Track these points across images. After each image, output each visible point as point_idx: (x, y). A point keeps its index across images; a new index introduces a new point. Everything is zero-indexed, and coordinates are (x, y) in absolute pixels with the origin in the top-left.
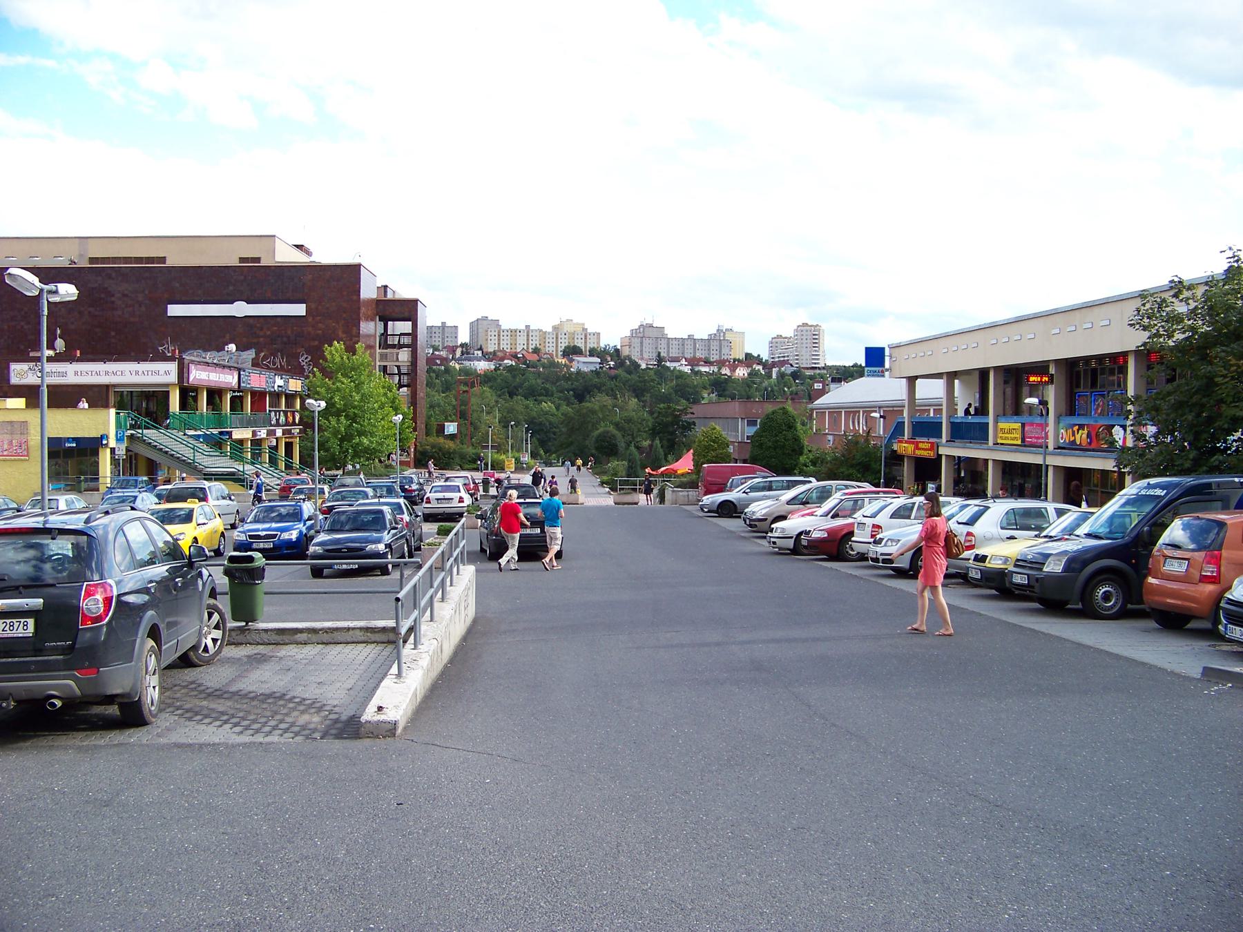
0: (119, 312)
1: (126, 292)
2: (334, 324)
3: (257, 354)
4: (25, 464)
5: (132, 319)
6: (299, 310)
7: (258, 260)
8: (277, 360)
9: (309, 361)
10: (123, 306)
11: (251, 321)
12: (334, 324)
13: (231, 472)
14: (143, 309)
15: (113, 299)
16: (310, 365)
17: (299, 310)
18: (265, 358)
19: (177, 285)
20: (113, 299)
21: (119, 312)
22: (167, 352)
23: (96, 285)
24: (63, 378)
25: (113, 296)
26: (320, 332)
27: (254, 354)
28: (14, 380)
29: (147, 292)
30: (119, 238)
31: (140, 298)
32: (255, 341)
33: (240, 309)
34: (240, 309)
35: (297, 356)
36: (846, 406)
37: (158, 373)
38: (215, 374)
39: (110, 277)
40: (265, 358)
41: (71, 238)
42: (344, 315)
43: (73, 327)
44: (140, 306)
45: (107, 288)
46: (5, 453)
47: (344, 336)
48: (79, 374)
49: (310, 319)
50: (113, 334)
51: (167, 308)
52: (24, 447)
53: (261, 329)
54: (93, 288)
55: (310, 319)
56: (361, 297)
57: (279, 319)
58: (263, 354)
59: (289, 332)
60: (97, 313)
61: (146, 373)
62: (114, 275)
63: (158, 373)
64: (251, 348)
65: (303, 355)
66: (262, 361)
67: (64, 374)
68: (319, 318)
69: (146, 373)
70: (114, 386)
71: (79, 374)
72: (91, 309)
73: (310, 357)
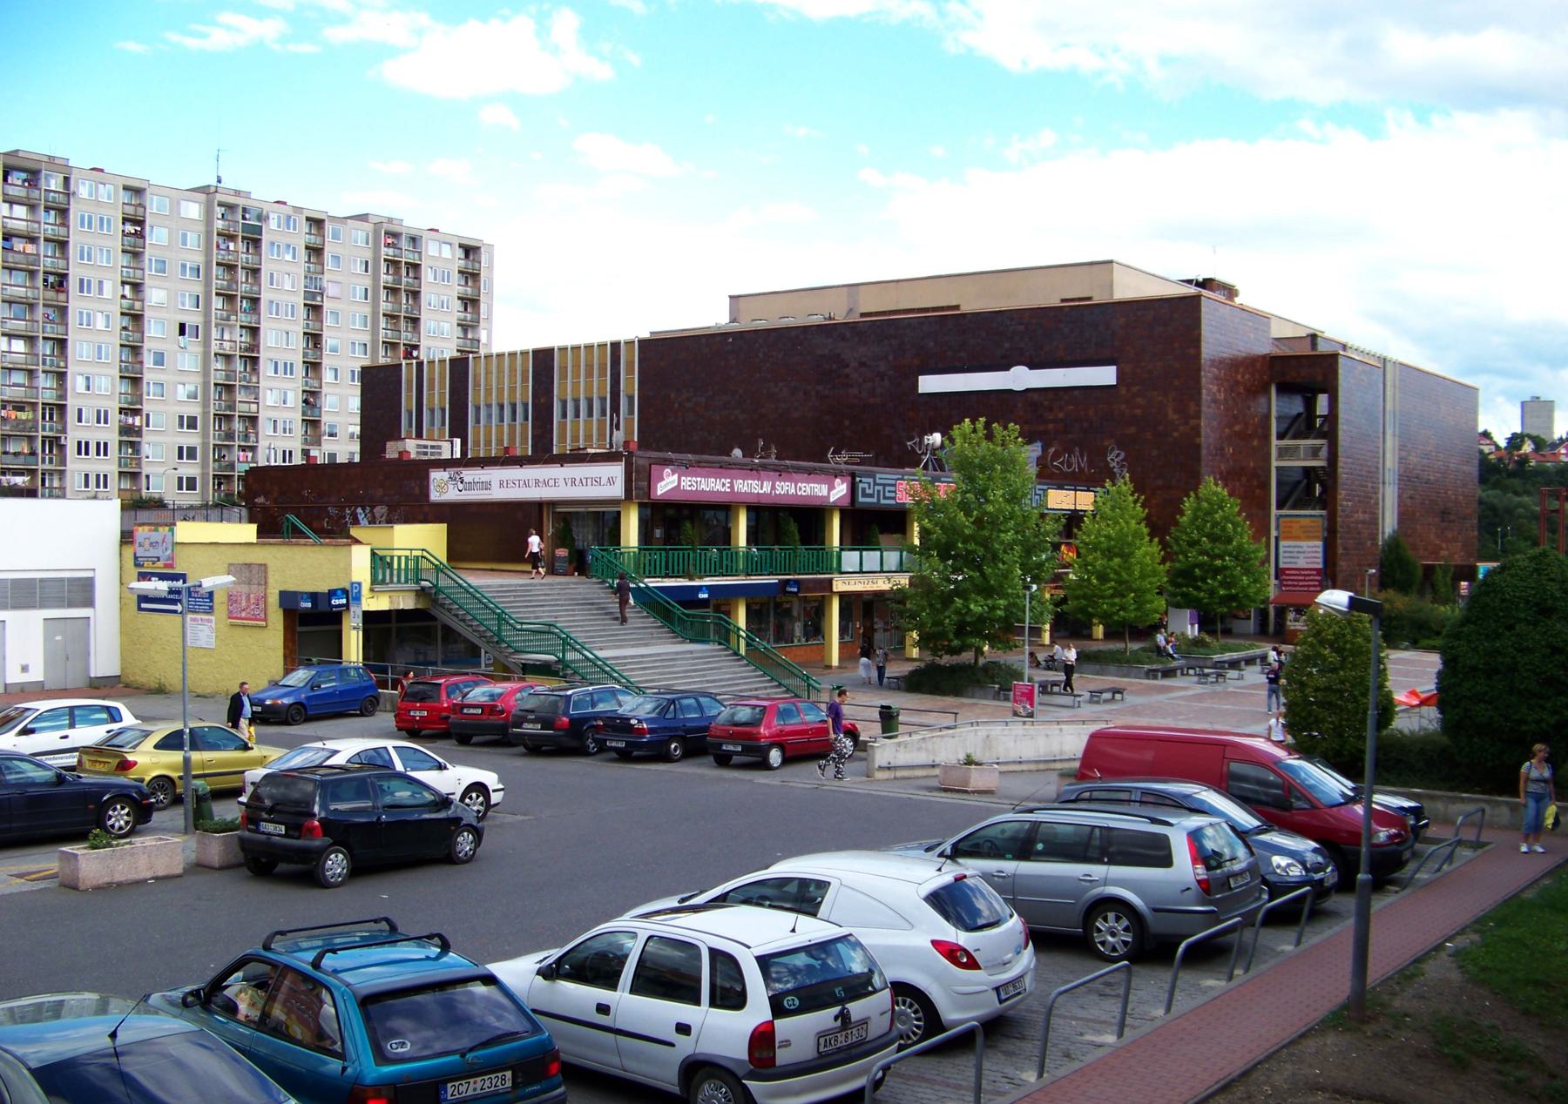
0: (855, 391)
1: (864, 360)
2: (1160, 398)
3: (1044, 449)
4: (257, 633)
5: (871, 400)
6: (1105, 376)
7: (957, 307)
8: (1074, 460)
9: (1122, 460)
10: (861, 380)
11: (1036, 396)
12: (1160, 398)
13: (545, 661)
14: (886, 383)
15: (847, 371)
16: (1123, 466)
17: (1105, 376)
18: (1056, 456)
19: (932, 344)
20: (847, 371)
21: (855, 391)
22: (917, 449)
23: (826, 352)
24: (482, 492)
25: (848, 366)
26: (1138, 412)
27: (1040, 449)
28: (435, 496)
29: (891, 358)
30: (898, 281)
31: (882, 367)
32: (1041, 428)
33: (1020, 378)
34: (1020, 378)
35: (1103, 453)
36: (519, 575)
37: (597, 481)
38: (713, 480)
39: (843, 338)
40: (1056, 456)
41: (838, 287)
42: (1176, 383)
43: (796, 415)
44: (882, 380)
45: (839, 355)
46: (243, 614)
47: (1176, 417)
48: (505, 485)
49: (1123, 391)
50: (847, 423)
51: (917, 381)
52: (262, 606)
53: (1051, 409)
54: (821, 356)
55: (1123, 391)
56: (1204, 356)
57: (1076, 393)
58: (1053, 449)
59: (1091, 413)
60: (827, 392)
61: (517, 483)
62: (848, 335)
63: (597, 481)
64: (1036, 442)
65: (1112, 450)
66: (1052, 461)
67: (486, 486)
68: (1137, 388)
69: (584, 481)
70: (553, 504)
71: (505, 485)
72: (819, 388)
73: (1123, 455)
